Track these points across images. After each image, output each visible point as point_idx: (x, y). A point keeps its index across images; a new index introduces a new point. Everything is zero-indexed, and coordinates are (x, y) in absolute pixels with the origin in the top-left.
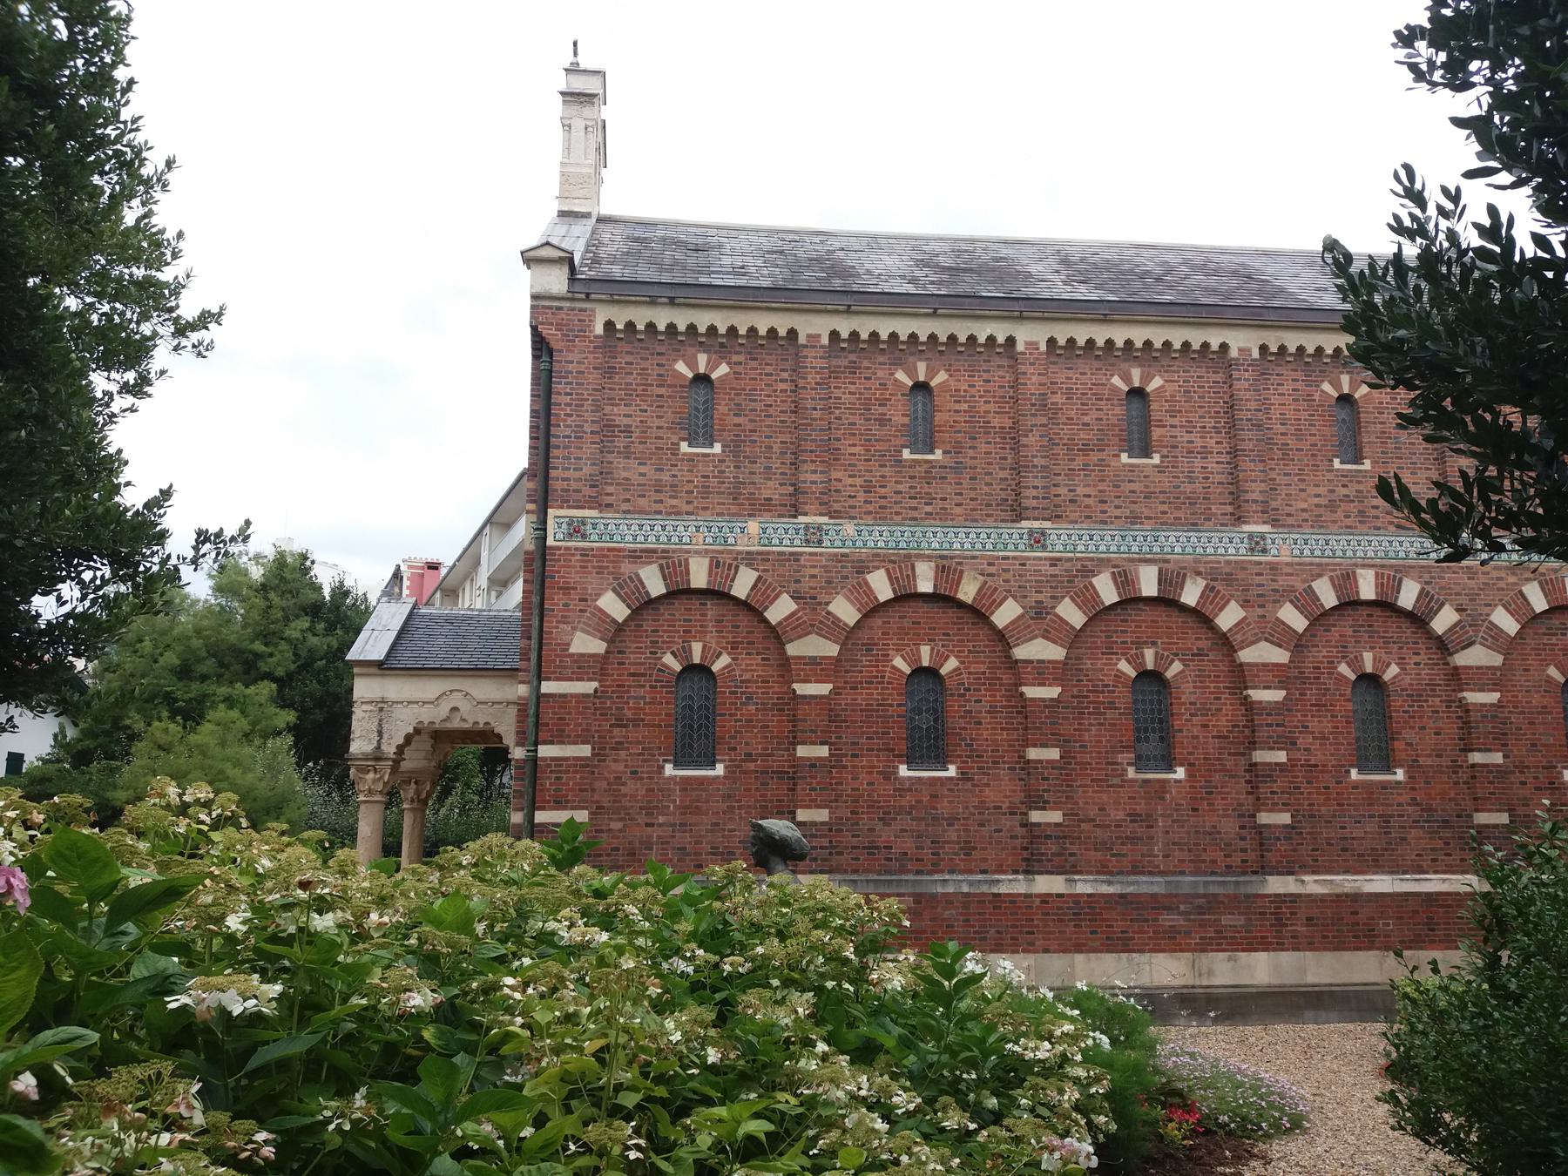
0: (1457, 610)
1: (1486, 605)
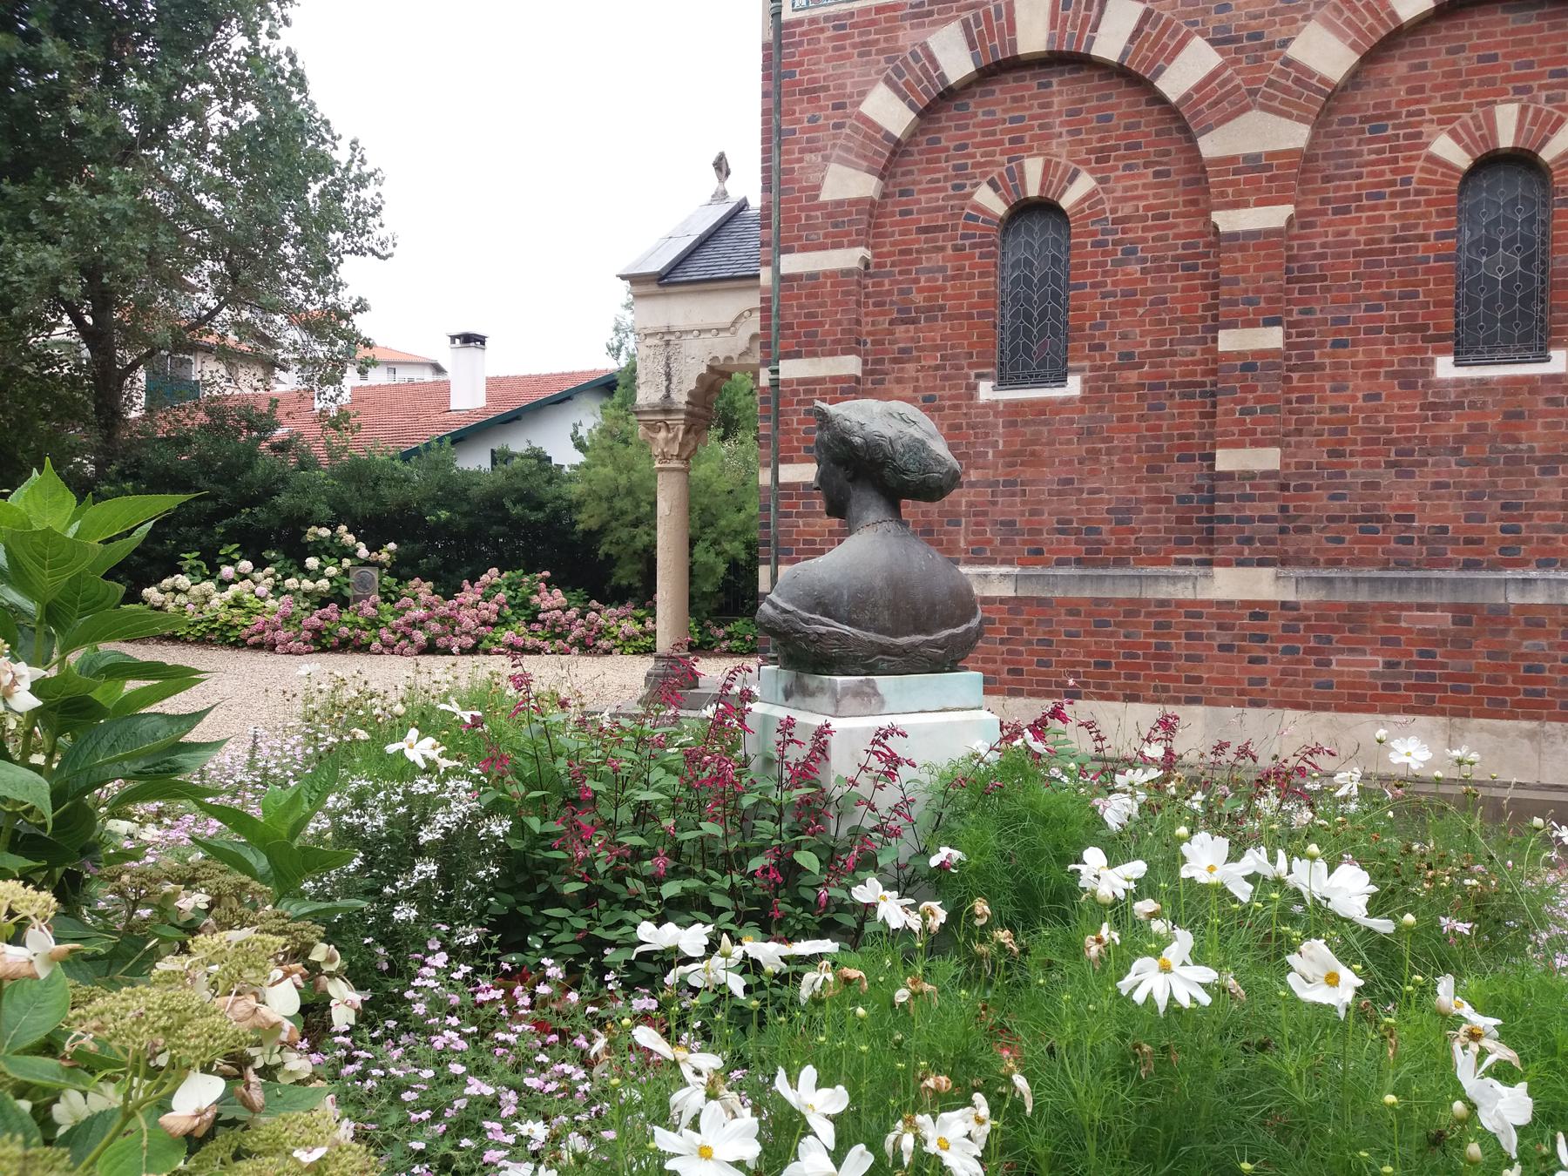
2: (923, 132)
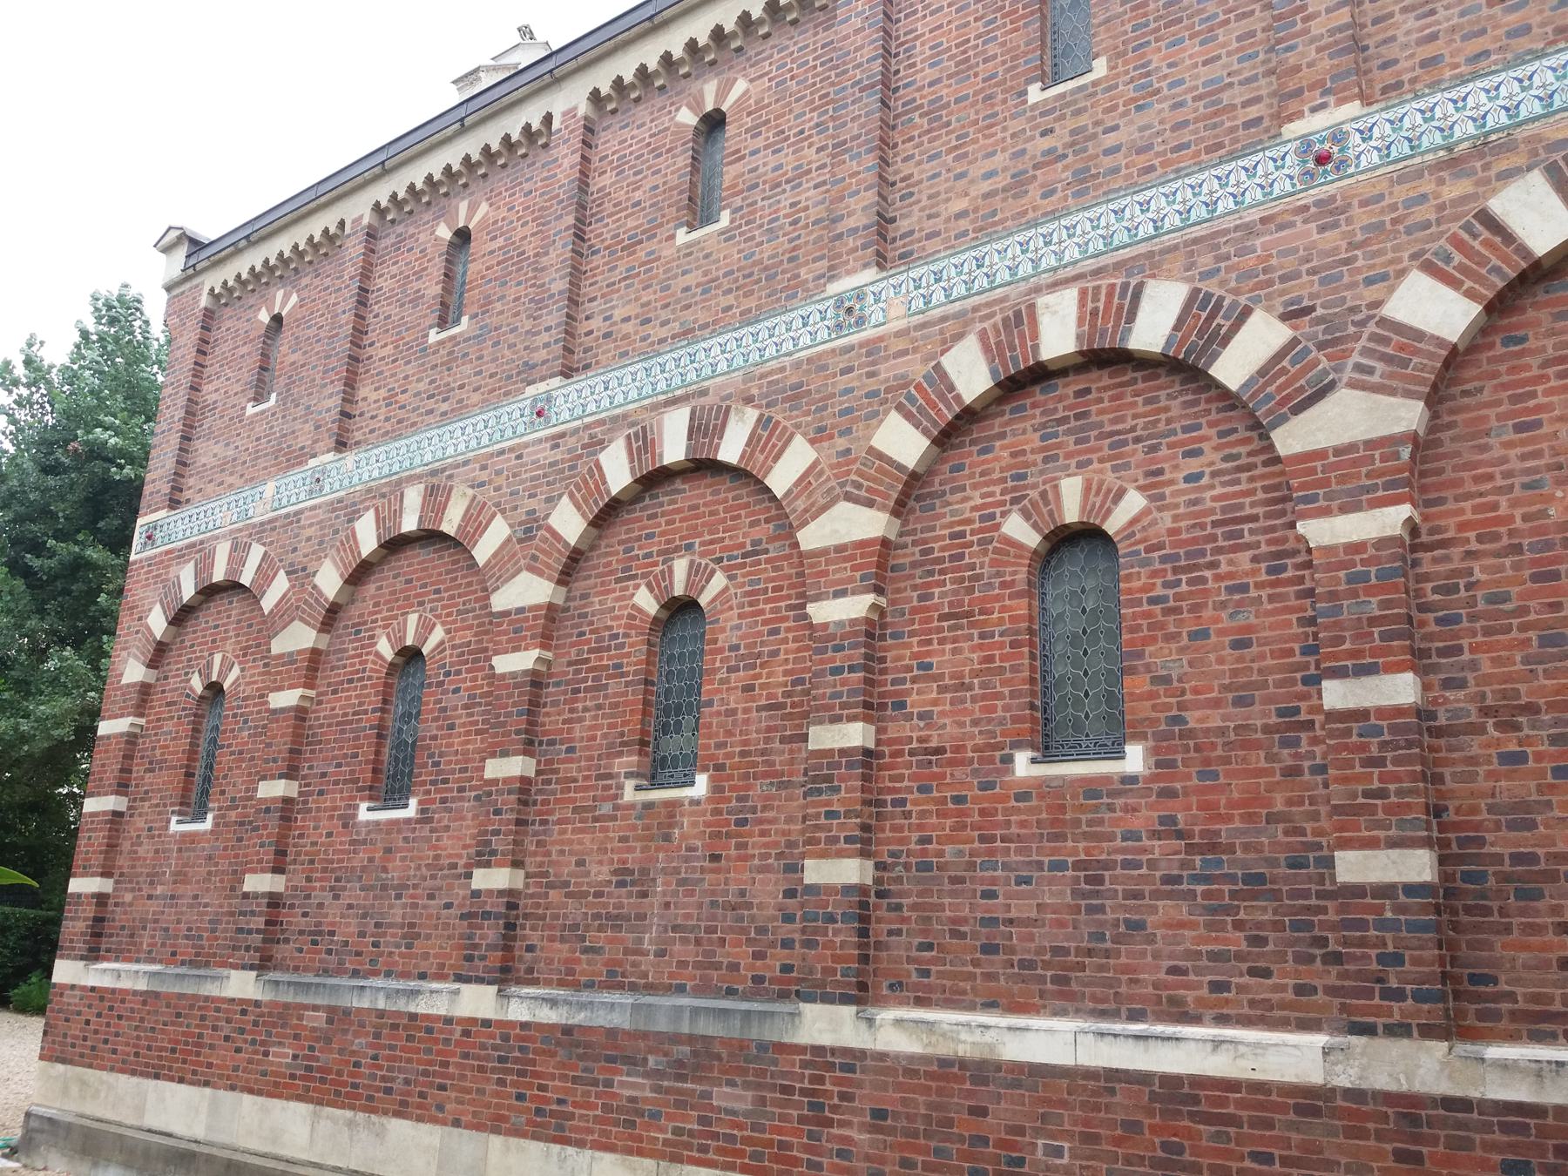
0: (1285, 317)
1: (1369, 282)
2: (944, 461)
